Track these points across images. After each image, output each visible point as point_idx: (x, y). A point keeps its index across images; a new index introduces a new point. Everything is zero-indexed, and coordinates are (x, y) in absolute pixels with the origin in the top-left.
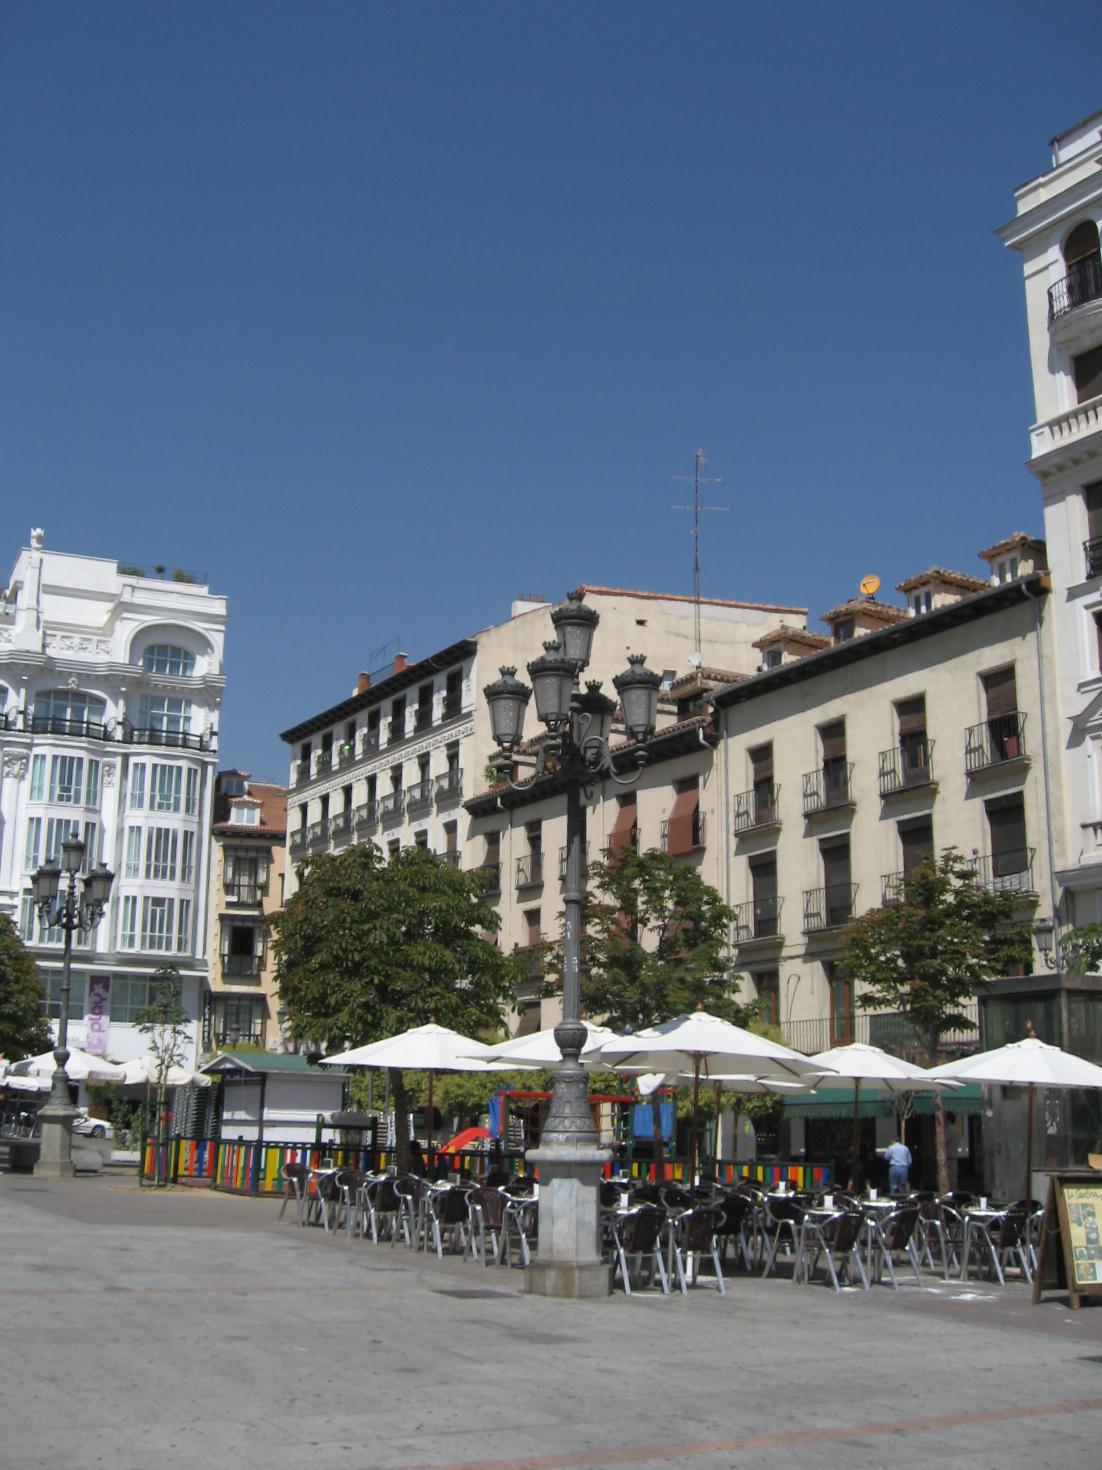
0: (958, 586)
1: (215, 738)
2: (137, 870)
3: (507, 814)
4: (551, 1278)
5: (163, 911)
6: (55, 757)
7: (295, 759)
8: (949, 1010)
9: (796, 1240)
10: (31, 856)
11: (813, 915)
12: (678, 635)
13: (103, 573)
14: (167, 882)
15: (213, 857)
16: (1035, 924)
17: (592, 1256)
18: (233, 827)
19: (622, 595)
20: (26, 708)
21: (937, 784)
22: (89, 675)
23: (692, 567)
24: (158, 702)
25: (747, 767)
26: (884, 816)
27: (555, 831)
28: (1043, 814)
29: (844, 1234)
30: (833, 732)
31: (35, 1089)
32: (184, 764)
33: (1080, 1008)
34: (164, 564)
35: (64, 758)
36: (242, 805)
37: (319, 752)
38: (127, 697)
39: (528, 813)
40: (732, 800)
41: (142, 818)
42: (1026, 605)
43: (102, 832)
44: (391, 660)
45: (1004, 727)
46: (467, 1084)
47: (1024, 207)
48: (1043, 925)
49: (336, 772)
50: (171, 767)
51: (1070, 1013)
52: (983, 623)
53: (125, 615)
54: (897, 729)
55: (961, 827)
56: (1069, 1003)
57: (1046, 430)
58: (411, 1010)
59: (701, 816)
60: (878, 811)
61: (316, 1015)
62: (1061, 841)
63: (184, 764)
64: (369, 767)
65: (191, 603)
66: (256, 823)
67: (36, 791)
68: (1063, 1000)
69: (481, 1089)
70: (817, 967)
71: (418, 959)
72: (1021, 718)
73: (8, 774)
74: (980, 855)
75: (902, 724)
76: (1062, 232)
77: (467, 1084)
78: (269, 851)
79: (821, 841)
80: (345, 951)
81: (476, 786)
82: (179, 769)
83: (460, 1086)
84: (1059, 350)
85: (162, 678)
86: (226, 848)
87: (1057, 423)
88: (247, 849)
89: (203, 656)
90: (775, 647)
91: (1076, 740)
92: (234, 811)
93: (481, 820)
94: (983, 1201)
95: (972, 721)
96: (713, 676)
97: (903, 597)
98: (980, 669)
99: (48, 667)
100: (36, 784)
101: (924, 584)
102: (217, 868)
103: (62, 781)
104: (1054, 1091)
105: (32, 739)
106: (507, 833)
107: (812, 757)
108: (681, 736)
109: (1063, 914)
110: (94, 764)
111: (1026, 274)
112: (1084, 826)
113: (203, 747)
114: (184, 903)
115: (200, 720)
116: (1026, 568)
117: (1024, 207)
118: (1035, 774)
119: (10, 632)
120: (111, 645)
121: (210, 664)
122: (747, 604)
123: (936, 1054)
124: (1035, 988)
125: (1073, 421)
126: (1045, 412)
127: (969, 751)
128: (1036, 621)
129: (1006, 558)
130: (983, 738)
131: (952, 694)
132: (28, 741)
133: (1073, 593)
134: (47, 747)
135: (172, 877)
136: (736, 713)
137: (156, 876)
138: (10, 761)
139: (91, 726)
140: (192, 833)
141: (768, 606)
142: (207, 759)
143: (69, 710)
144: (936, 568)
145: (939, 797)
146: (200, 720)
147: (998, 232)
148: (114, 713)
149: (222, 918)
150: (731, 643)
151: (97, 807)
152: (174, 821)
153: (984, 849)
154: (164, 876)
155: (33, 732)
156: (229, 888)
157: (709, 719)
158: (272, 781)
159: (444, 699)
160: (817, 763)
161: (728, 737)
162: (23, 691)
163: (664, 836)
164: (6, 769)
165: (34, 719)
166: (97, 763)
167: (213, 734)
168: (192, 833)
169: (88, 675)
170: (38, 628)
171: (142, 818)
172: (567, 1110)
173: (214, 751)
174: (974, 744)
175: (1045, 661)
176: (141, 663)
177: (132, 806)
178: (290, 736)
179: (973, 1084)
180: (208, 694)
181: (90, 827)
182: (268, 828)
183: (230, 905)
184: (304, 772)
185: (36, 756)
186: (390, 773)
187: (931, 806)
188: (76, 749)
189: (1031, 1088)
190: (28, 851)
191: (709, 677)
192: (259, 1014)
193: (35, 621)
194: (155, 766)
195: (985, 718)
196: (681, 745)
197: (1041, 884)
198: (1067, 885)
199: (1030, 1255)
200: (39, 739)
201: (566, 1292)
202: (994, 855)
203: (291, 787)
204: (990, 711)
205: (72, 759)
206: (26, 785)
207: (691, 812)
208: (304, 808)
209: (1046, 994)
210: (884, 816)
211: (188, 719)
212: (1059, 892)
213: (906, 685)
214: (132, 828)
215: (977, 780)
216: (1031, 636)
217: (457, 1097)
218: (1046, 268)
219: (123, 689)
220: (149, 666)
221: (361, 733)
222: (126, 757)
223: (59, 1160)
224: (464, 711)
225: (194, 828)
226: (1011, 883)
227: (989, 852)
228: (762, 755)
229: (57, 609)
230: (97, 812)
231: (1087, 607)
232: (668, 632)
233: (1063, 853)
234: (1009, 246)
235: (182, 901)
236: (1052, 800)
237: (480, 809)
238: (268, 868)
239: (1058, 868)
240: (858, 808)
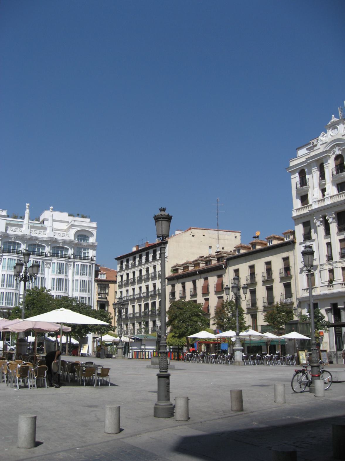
1: (95, 257)
2: (77, 290)
3: (177, 280)
4: (237, 363)
5: (84, 300)
6: (57, 263)
7: (119, 264)
8: (281, 327)
10: (53, 287)
12: (212, 238)
13: (64, 216)
14: (85, 293)
15: (95, 286)
16: (294, 308)
17: (242, 361)
18: (99, 279)
19: (199, 229)
20: (50, 251)
22: (65, 243)
24: (81, 249)
25: (233, 274)
29: (271, 358)
31: (75, 344)
32: (88, 264)
33: (301, 326)
34: (79, 213)
35: (60, 263)
36: (101, 274)
37: (126, 263)
38: (74, 248)
39: (182, 280)
40: (230, 281)
41: (79, 277)
42: (291, 245)
43: (69, 281)
44: (144, 242)
45: (287, 269)
46: (173, 341)
47: (292, 164)
48: (295, 308)
49: (130, 268)
50: (85, 265)
52: (283, 248)
53: (73, 227)
54: (266, 268)
55: (279, 289)
56: (300, 324)
57: (295, 211)
58: (193, 328)
59: (223, 283)
61: (178, 329)
62: (298, 292)
63: (88, 264)
64: (140, 268)
65: (86, 223)
66: (105, 278)
67: (53, 271)
69: (176, 342)
70: (249, 315)
71: (194, 320)
73: (46, 267)
74: (283, 294)
76: (298, 171)
77: (173, 341)
78: (108, 285)
81: (168, 274)
82: (87, 265)
83: (172, 341)
85: (82, 243)
86: (98, 284)
87: (298, 210)
88: (103, 285)
89: (91, 237)
90: (239, 248)
91: (301, 272)
92: (99, 275)
93: (170, 282)
94: (288, 355)
95: (281, 268)
98: (283, 257)
99: (56, 241)
100: (53, 270)
101: (271, 238)
102: (96, 289)
103: (59, 269)
104: (297, 340)
105: (52, 259)
108: (219, 266)
109: (299, 306)
110: (67, 264)
111: (292, 178)
112: (303, 289)
113: (92, 260)
114: (89, 298)
115: (91, 253)
116: (291, 237)
117: (292, 164)
118: (293, 278)
119: (46, 232)
120: (70, 235)
121: (93, 239)
122: (227, 231)
125: (300, 209)
126: (295, 207)
127: (280, 273)
128: (293, 248)
129: (287, 235)
130: (283, 271)
131: (277, 262)
132: (51, 259)
133: (301, 244)
134: (55, 260)
135: (86, 292)
136: (231, 262)
137: (82, 291)
138: (47, 264)
139: (66, 255)
140: (90, 281)
142: (93, 263)
143: (60, 251)
144: (273, 235)
145: (274, 282)
146: (91, 253)
147: (286, 169)
148: (71, 252)
149: (98, 301)
151: (67, 275)
152: (86, 278)
153: (283, 293)
154: (84, 292)
155: (52, 257)
156: (99, 294)
157: (225, 263)
159: (160, 253)
161: (229, 267)
162: (49, 247)
163: (215, 287)
164: (46, 266)
165: (52, 254)
166: (67, 264)
167: (94, 256)
168: (90, 281)
169: (65, 243)
170: (53, 231)
171: (79, 277)
172: (238, 342)
173: (95, 261)
174: (281, 272)
175: (295, 257)
176: (77, 239)
177: (76, 275)
178: (117, 259)
179: (285, 338)
180: (93, 247)
181: (66, 280)
182: (108, 279)
183: (99, 298)
184: (121, 268)
185: (53, 263)
186: (145, 269)
188: (62, 261)
189: (294, 339)
190: (52, 286)
191: (224, 254)
193: (52, 229)
194: (81, 265)
195: (283, 267)
196: (218, 268)
197: (294, 300)
198: (300, 300)
200: (53, 259)
201: (239, 365)
203: (118, 271)
204: (284, 266)
205: (61, 263)
206: (51, 270)
208: (122, 276)
209: (296, 323)
211: (88, 253)
212: (298, 302)
213: (268, 259)
214: (76, 280)
215: (282, 279)
217: (171, 343)
218: (295, 177)
219: (73, 246)
220: (78, 239)
221: (137, 259)
222: (74, 262)
223: (121, 356)
225: (91, 280)
226: (289, 300)
227: (284, 294)
228: (237, 271)
229: (57, 225)
230: (68, 276)
231: (303, 247)
233: (299, 294)
234: (288, 172)
235: (88, 298)
236: (296, 284)
238: (108, 289)
239: (298, 297)
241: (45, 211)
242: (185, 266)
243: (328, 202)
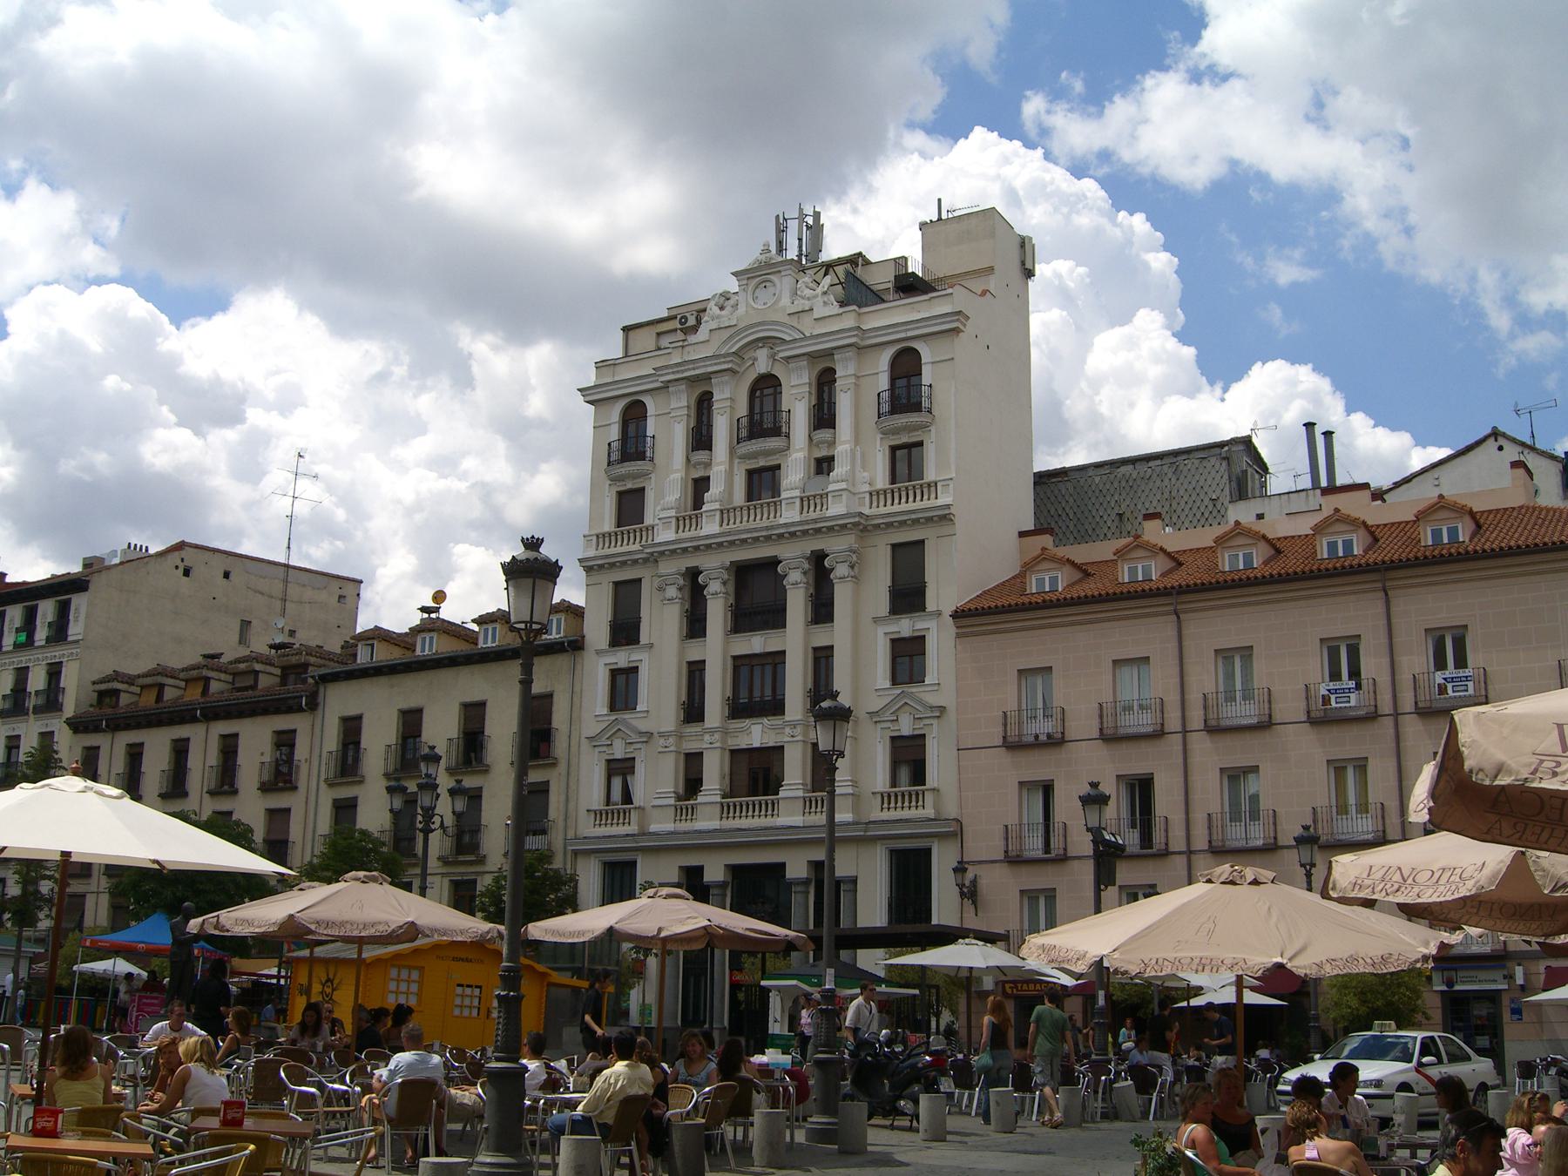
12: (256, 592)
118: (562, 767)
241: (1199, 186)
242: (156, 679)
243: (710, 527)
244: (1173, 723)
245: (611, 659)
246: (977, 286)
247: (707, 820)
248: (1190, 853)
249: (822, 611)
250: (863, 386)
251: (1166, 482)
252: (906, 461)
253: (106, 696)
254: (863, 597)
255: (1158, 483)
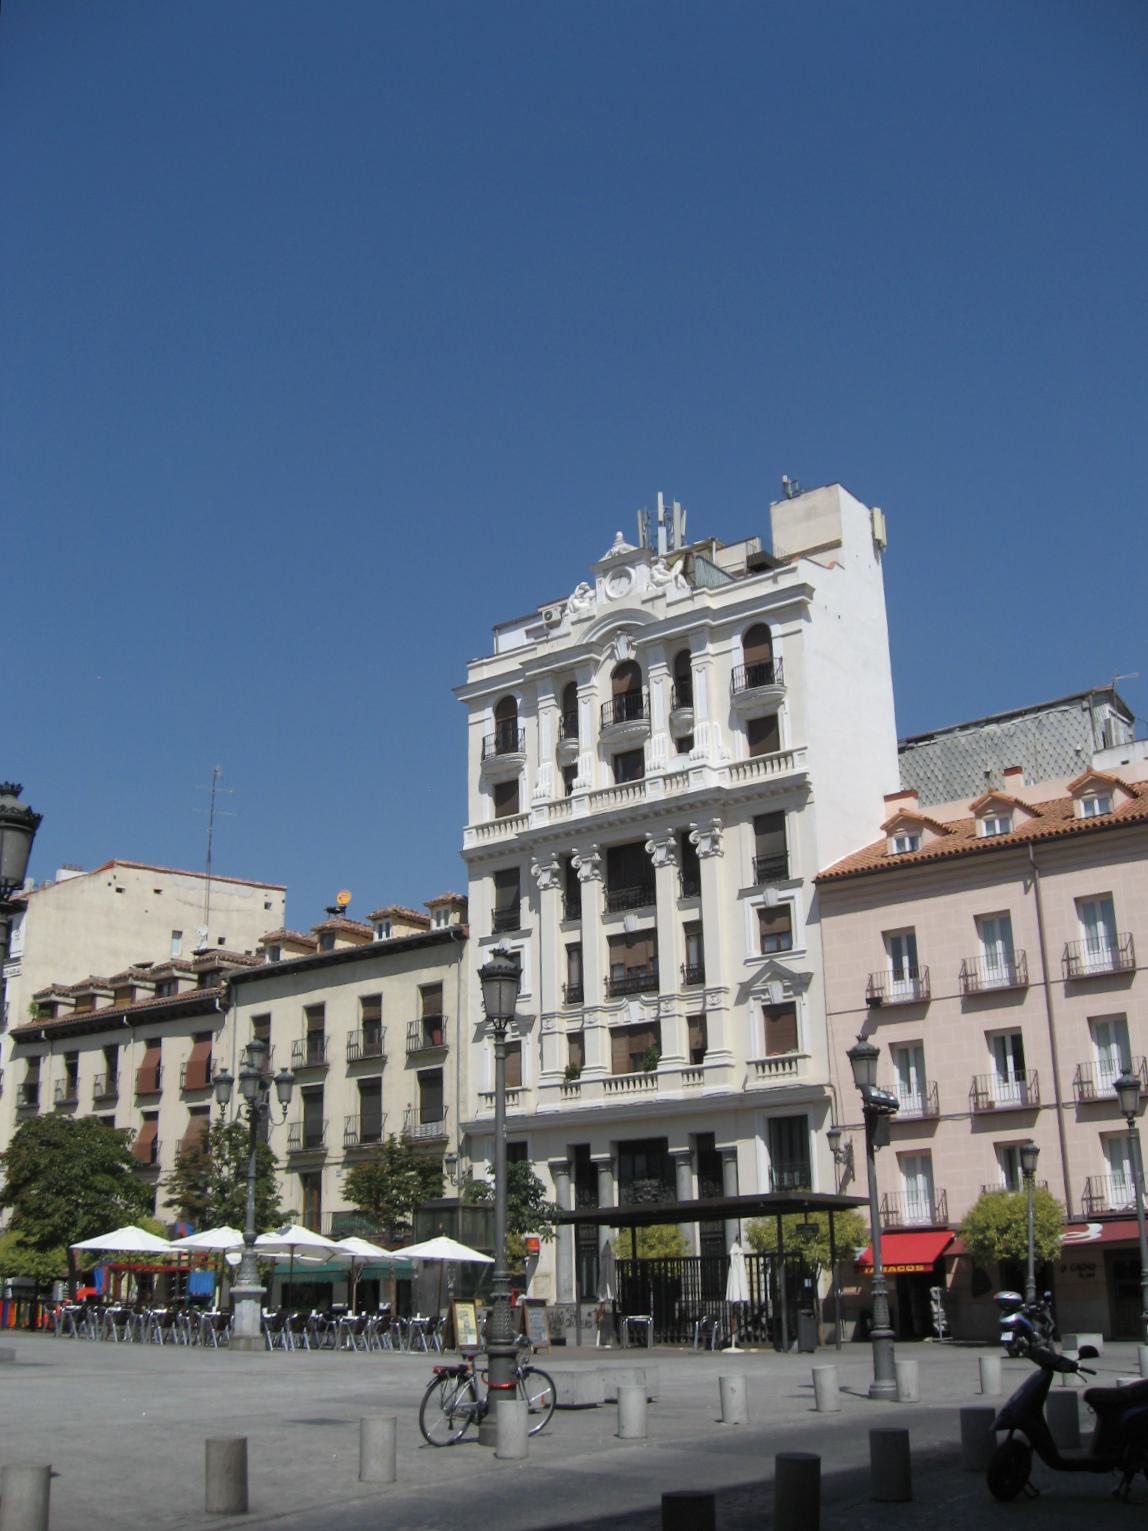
0: (409, 920)
3: (48, 1044)
4: (242, 1343)
8: (400, 1219)
9: (336, 1331)
11: (294, 1140)
12: (185, 903)
16: (446, 1157)
17: (258, 1333)
19: (145, 868)
21: (386, 1057)
23: (206, 857)
26: (349, 1075)
27: (92, 1062)
28: (455, 1084)
29: (360, 1327)
30: (316, 1012)
33: (469, 1217)
39: (69, 1044)
45: (433, 1023)
47: (474, 676)
51: (463, 1220)
52: (424, 951)
55: (400, 1090)
57: (474, 831)
60: (345, 1072)
62: (465, 1102)
68: (460, 1213)
70: (296, 1177)
71: (100, 1186)
72: (444, 1019)
75: (365, 1013)
79: (303, 1088)
80: (56, 1179)
83: (14, 1261)
84: (487, 779)
87: (482, 828)
89: (349, 1182)
90: (275, 944)
91: (478, 1038)
93: (23, 1046)
95: (413, 1019)
96: (227, 958)
97: (370, 923)
104: (453, 1263)
106: (48, 1058)
107: (299, 1028)
108: (202, 1002)
109: (464, 1150)
111: (470, 721)
116: (454, 918)
118: (451, 1057)
123: (395, 1244)
124: (445, 1205)
126: (474, 820)
127: (409, 1037)
128: (458, 956)
129: (442, 909)
130: (419, 1030)
136: (244, 989)
141: (257, 883)
145: (387, 1066)
150: (227, 911)
157: (224, 992)
158: (571, 1289)
160: (303, 1033)
161: (237, 1005)
172: (249, 1270)
174: (413, 1033)
175: (462, 985)
187: (381, 1071)
189: (441, 1262)
191: (223, 959)
192: (1101, 1306)
195: (420, 1017)
197: (450, 1131)
199: (439, 1339)
201: (249, 1348)
202: (422, 1109)
204: (424, 1012)
207: (205, 1058)
209: (452, 1208)
210: (349, 1075)
212: (462, 1136)
213: (370, 987)
215: (413, 1057)
216: (455, 965)
217: (11, 1269)
224: (12, 956)
226: (433, 1130)
227: (419, 1106)
228: (262, 1022)
232: (179, 900)
233: (466, 1111)
237: (22, 1037)
239: (462, 1121)
240: (331, 1068)
242: (84, 995)
243: (581, 811)
244: (1036, 976)
245: (759, 898)
246: (824, 558)
247: (592, 1098)
248: (1058, 1106)
249: (691, 884)
250: (718, 668)
251: (1031, 737)
252: (762, 732)
253: (45, 1005)
254: (731, 856)
255: (1023, 738)
